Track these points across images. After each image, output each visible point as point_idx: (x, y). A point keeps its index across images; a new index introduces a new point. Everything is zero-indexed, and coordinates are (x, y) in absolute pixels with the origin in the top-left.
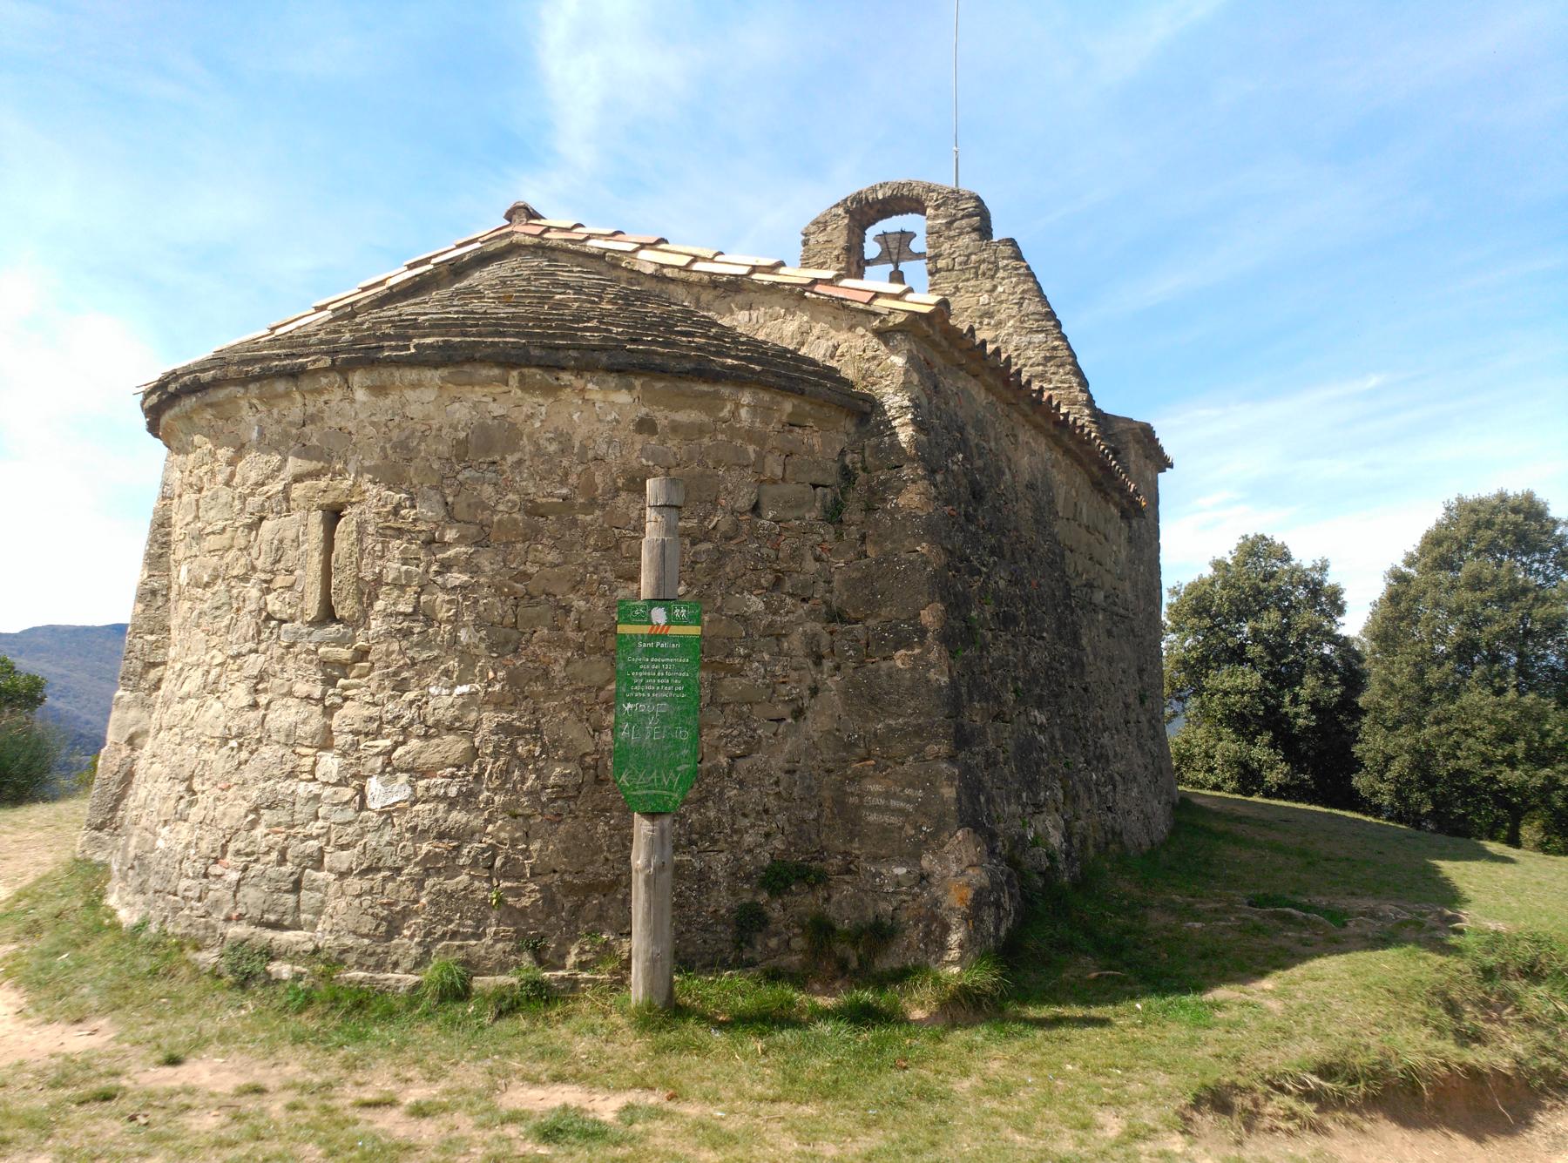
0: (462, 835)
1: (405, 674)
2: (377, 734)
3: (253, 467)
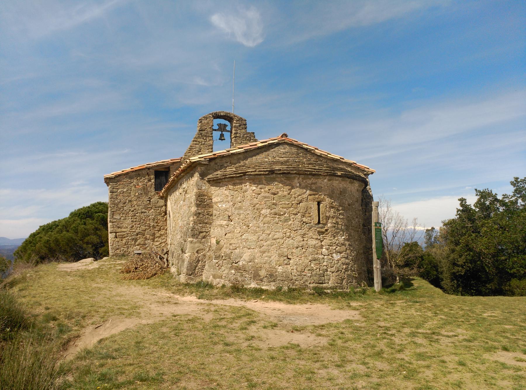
3: (297, 191)
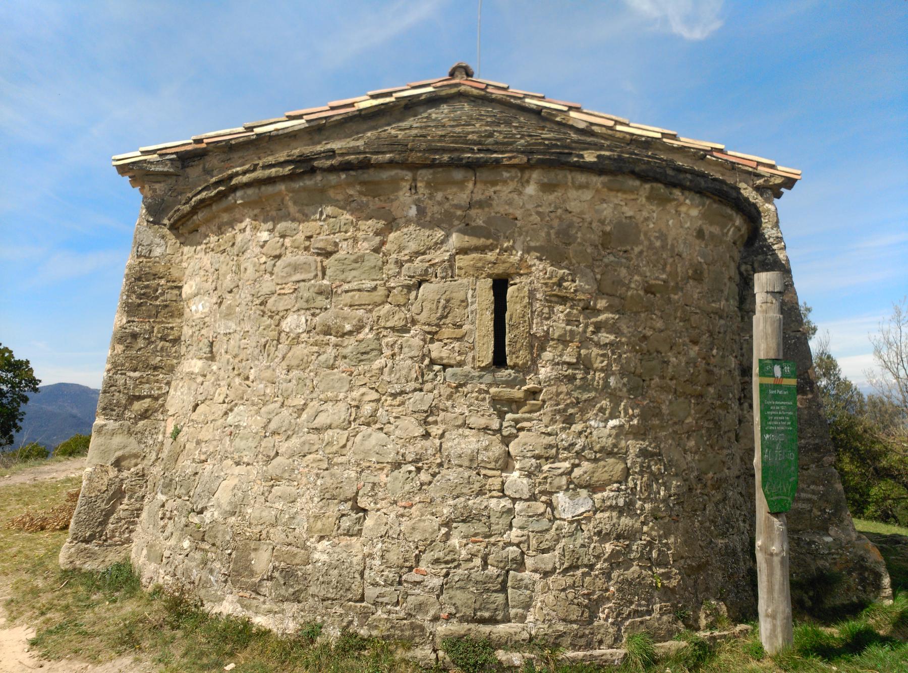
0: (629, 536)
1: (571, 411)
2: (555, 458)
3: (408, 238)
